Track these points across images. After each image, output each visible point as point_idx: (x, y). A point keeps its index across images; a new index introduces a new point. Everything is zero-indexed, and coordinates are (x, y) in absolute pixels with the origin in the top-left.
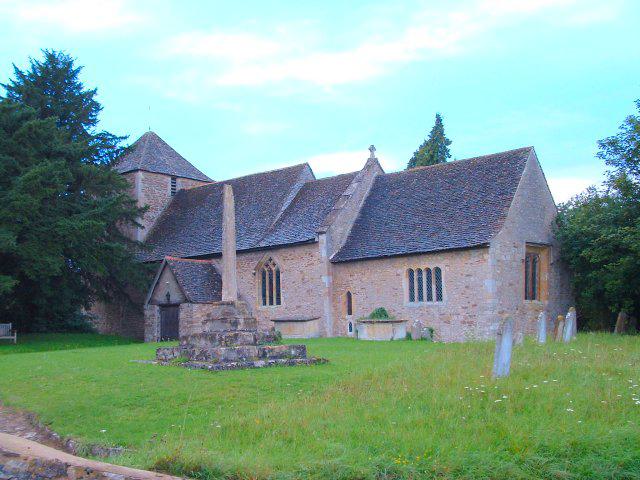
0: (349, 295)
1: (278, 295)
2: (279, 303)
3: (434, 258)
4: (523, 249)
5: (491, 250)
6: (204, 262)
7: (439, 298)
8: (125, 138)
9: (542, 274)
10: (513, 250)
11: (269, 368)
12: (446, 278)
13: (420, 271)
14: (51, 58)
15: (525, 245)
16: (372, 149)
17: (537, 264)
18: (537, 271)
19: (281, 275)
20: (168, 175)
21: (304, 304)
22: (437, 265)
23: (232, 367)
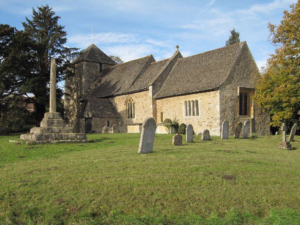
1: (198, 110)
6: (106, 100)
7: (198, 114)
11: (86, 143)
12: (200, 105)
13: (189, 101)
16: (178, 47)
19: (135, 105)
20: (98, 63)
22: (197, 99)
23: (69, 142)
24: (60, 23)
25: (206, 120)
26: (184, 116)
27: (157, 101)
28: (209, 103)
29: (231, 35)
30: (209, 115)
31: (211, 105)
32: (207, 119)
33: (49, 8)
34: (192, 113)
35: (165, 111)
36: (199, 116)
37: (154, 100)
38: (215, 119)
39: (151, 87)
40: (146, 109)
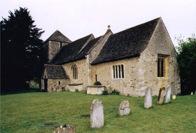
0: (96, 75)
1: (77, 77)
2: (77, 79)
3: (121, 61)
4: (156, 57)
5: (141, 57)
7: (123, 77)
8: (41, 29)
9: (166, 66)
10: (152, 57)
12: (125, 69)
14: (21, 9)
15: (157, 55)
17: (164, 63)
18: (164, 66)
19: (78, 69)
20: (59, 41)
21: (83, 79)
22: (122, 64)
25: (130, 81)
27: (89, 88)
28: (132, 67)
30: (133, 77)
31: (134, 69)
34: (115, 77)
35: (98, 73)
36: (124, 78)
40: (85, 73)
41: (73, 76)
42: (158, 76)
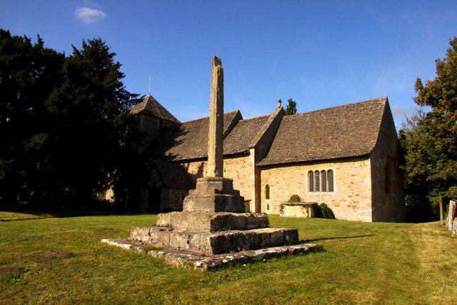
7: (331, 190)
24: (115, 60)
25: (347, 198)
26: (306, 193)
28: (353, 175)
29: (288, 104)
31: (356, 178)
32: (268, 206)
33: (103, 42)
34: (321, 189)
35: (274, 183)
37: (258, 170)
38: (365, 197)
39: (252, 151)
41: (292, 259)
42: (311, 190)
